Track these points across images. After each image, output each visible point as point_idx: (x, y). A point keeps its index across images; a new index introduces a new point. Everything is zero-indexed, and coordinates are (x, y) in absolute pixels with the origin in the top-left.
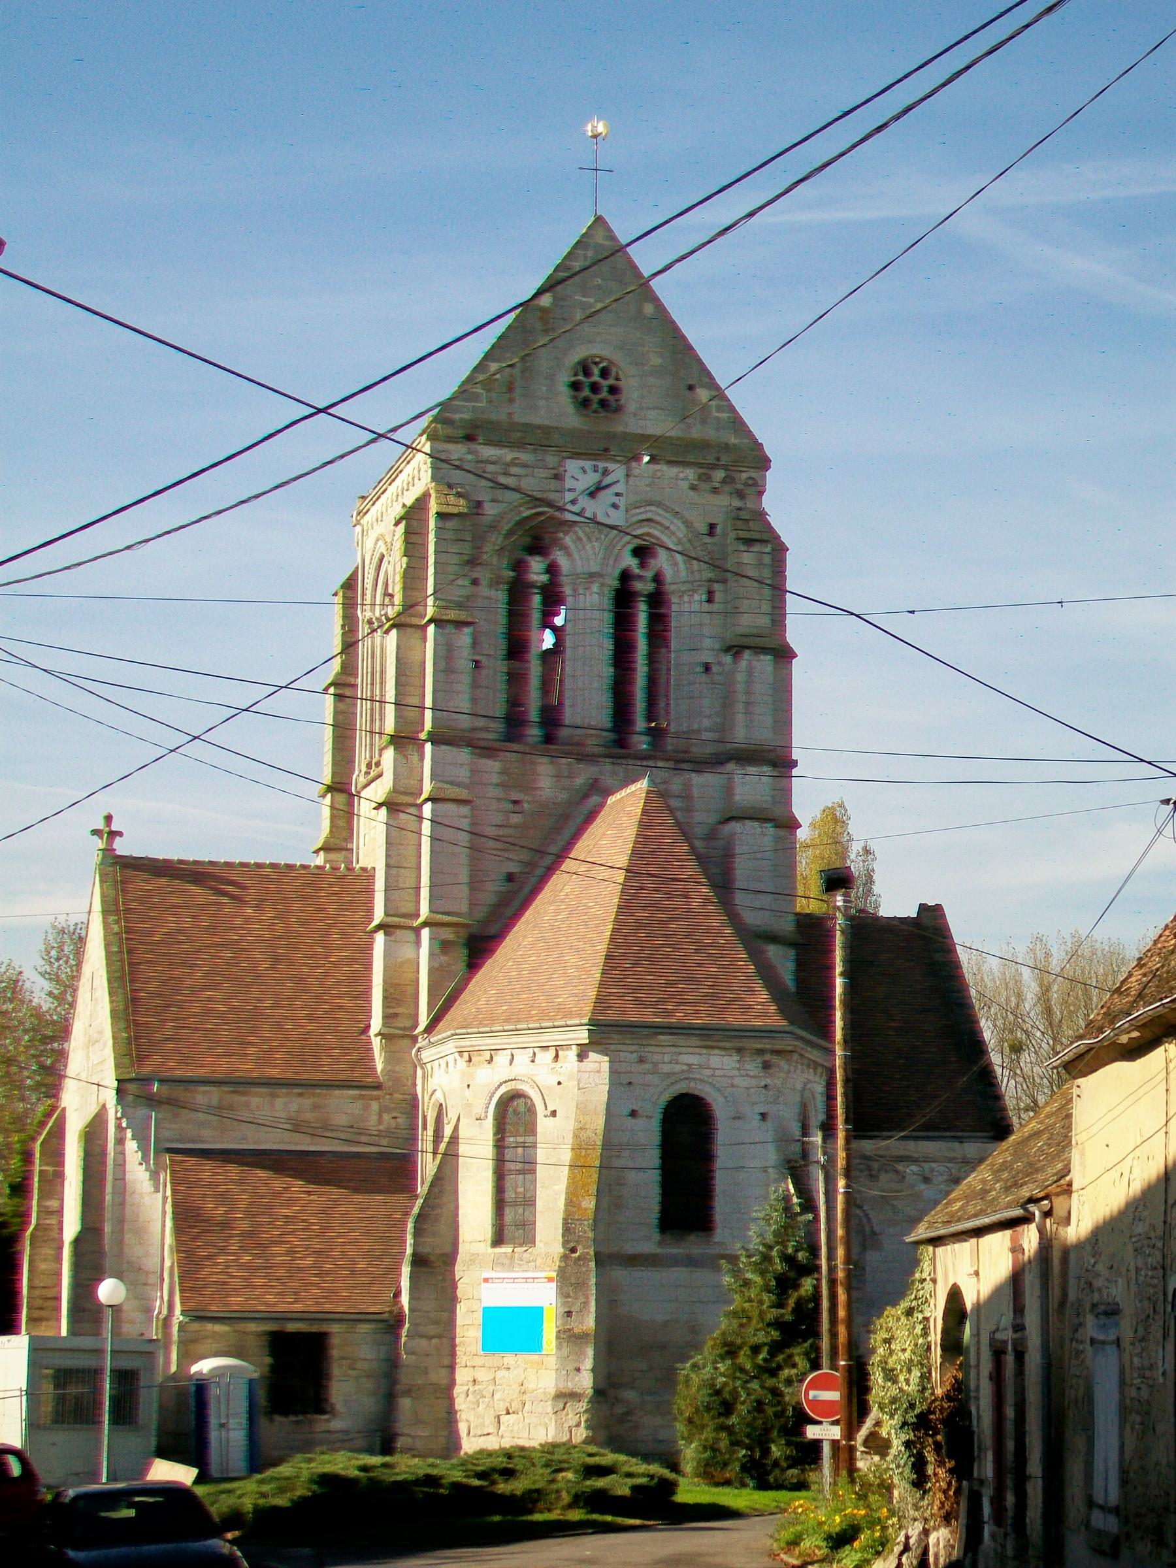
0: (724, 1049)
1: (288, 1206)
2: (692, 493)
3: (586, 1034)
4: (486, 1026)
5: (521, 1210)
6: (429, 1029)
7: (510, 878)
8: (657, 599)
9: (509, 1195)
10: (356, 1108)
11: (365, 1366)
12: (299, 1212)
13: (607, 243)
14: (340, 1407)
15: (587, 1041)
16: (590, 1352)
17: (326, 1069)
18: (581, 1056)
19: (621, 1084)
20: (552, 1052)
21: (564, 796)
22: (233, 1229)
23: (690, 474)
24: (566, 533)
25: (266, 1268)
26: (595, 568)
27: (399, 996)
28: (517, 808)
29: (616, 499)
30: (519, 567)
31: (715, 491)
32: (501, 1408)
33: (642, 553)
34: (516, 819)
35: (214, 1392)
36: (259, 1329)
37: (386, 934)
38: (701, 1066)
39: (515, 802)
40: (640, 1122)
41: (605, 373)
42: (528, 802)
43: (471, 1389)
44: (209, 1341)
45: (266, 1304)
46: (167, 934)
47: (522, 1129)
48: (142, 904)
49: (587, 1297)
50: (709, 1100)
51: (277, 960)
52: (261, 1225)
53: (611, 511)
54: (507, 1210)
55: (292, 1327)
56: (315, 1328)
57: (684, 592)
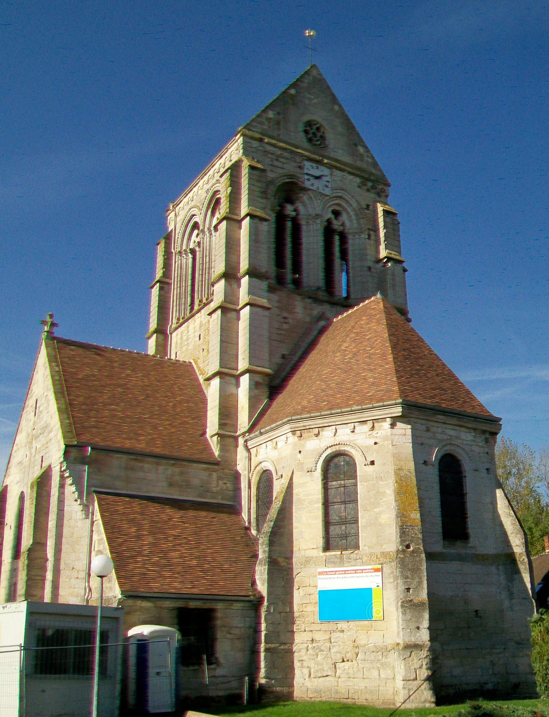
1: (174, 529)
2: (359, 189)
3: (400, 409)
5: (343, 527)
6: (251, 429)
7: (283, 356)
8: (343, 238)
9: (334, 518)
10: (204, 475)
11: (236, 631)
12: (181, 533)
13: (318, 76)
14: (222, 660)
15: (400, 414)
16: (426, 616)
17: (185, 452)
18: (393, 425)
19: (417, 443)
20: (370, 424)
21: (308, 319)
22: (143, 540)
23: (358, 180)
24: (304, 194)
25: (169, 565)
26: (319, 212)
27: (228, 413)
28: (286, 321)
29: (327, 183)
30: (282, 206)
31: (368, 190)
32: (339, 657)
33: (336, 214)
34: (286, 326)
35: (151, 648)
36: (171, 606)
38: (456, 437)
39: (285, 318)
40: (429, 468)
41: (318, 129)
43: (310, 646)
44: (139, 613)
45: (175, 588)
46: (85, 375)
47: (342, 476)
48: (70, 360)
49: (421, 578)
50: (460, 458)
51: (148, 396)
52: (160, 539)
53: (325, 188)
54: (332, 528)
55: (193, 605)
56: (208, 605)
57: (356, 233)
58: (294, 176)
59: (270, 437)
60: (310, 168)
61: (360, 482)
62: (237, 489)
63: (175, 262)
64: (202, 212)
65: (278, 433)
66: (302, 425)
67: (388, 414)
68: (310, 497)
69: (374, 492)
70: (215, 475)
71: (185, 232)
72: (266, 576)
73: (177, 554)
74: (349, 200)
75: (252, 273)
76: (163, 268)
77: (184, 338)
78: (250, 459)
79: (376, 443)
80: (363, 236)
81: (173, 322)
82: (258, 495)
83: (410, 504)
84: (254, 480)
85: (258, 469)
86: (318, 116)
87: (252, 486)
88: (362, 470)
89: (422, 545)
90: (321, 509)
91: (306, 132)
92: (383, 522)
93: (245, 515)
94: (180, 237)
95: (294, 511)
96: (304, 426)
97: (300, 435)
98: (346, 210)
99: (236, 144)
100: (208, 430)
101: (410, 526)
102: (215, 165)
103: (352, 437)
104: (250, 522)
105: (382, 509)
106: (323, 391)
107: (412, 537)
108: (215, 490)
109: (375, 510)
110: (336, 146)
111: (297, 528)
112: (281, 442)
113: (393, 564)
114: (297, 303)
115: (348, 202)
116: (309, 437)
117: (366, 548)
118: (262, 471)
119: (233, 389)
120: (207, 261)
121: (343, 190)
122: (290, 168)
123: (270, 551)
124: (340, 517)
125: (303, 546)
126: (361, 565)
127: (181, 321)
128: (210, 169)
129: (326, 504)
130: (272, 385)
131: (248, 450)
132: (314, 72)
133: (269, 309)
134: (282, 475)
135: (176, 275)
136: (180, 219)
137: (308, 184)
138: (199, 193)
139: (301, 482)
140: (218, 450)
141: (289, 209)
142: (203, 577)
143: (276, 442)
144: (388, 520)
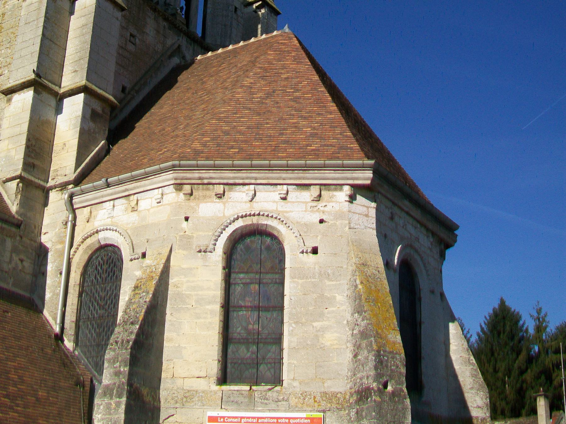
0: (428, 229)
4: (228, 157)
9: (237, 330)
15: (368, 182)
18: (352, 198)
20: (315, 191)
34: (131, 47)
37: (35, 91)
39: (132, 35)
42: (139, 40)
50: (417, 270)
59: (126, 190)
61: (292, 278)
62: (40, 273)
65: (145, 186)
66: (197, 175)
67: (348, 179)
68: (200, 293)
69: (315, 296)
72: (123, 416)
79: (321, 221)
82: (82, 285)
83: (385, 319)
84: (79, 259)
85: (89, 241)
88: (292, 259)
89: (405, 385)
90: (218, 314)
92: (328, 344)
93: (51, 314)
95: (168, 311)
96: (200, 178)
97: (190, 192)
101: (390, 352)
103: (282, 206)
104: (62, 328)
105: (326, 323)
106: (227, 133)
107: (392, 370)
109: (315, 324)
111: (171, 340)
112: (147, 202)
113: (342, 412)
116: (205, 197)
117: (296, 384)
118: (97, 246)
119: (49, 113)
123: (131, 374)
124: (249, 332)
125: (180, 371)
126: (285, 411)
129: (227, 308)
130: (118, 119)
133: (122, 9)
134: (144, 255)
139: (184, 266)
140: (16, 203)
142: (11, 408)
143: (138, 201)
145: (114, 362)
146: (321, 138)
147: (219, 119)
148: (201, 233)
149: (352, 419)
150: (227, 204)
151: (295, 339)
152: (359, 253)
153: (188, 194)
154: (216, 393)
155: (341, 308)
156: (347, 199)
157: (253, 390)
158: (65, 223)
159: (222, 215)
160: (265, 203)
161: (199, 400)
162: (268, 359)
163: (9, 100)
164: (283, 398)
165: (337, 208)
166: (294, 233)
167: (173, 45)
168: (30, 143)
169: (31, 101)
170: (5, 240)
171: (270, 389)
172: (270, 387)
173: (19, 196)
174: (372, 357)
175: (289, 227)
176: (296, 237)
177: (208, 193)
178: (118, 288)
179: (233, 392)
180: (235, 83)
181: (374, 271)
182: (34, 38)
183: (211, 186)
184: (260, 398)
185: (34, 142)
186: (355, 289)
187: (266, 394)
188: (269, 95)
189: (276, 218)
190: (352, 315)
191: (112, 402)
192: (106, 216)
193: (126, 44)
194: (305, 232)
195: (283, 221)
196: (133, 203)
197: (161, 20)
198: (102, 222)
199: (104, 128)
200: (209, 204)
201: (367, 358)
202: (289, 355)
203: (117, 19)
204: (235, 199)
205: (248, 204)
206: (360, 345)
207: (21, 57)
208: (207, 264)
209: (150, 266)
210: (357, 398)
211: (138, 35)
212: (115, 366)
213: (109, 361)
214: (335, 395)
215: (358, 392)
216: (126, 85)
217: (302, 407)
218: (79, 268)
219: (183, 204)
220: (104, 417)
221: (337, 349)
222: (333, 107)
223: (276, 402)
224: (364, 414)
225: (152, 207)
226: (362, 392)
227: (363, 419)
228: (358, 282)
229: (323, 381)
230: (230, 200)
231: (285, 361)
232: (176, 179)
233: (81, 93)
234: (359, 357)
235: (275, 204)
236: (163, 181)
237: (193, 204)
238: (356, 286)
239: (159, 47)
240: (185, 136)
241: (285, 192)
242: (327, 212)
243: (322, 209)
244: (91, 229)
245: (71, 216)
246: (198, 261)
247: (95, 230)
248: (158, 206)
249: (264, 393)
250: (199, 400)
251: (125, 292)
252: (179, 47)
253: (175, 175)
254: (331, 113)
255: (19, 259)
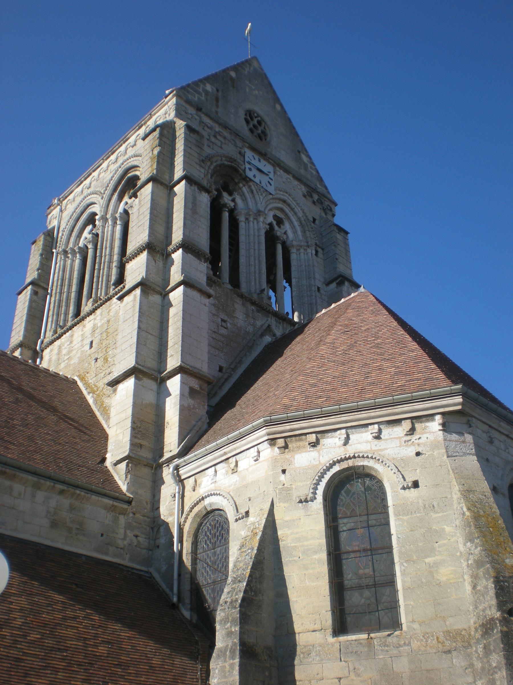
2: (304, 199)
6: (184, 452)
9: (349, 578)
15: (459, 407)
20: (407, 425)
23: (304, 188)
28: (224, 324)
34: (223, 331)
37: (136, 378)
39: (223, 320)
41: (259, 123)
42: (230, 323)
58: (235, 161)
59: (225, 454)
60: (252, 158)
61: (396, 515)
63: (56, 264)
64: (104, 196)
68: (305, 543)
70: (122, 520)
71: (74, 227)
72: (237, 677)
73: (70, 632)
74: (294, 207)
75: (186, 246)
76: (38, 270)
77: (64, 352)
78: (183, 497)
79: (418, 454)
80: (309, 251)
81: (47, 332)
85: (196, 509)
86: (261, 109)
87: (185, 538)
91: (247, 122)
92: (444, 579)
94: (66, 233)
97: (283, 445)
98: (289, 218)
99: (166, 107)
100: (108, 456)
102: (129, 138)
108: (120, 543)
109: (427, 560)
110: (278, 145)
112: (246, 462)
114: (237, 306)
115: (292, 209)
116: (299, 448)
118: (204, 513)
120: (107, 253)
121: (287, 193)
122: (230, 150)
127: (59, 331)
128: (121, 145)
131: (180, 481)
132: (255, 64)
134: (247, 513)
135: (56, 279)
136: (66, 215)
137: (250, 174)
138: (101, 176)
139: (287, 518)
141: (226, 198)
143: (237, 462)
144: (452, 576)
145: (225, 623)
146: (406, 374)
147: (307, 375)
148: (299, 484)
149: (481, 656)
150: (321, 452)
151: (408, 579)
152: (462, 480)
153: (283, 447)
154: (333, 645)
155: (452, 540)
156: (441, 428)
157: (371, 638)
158: (173, 496)
159: (318, 463)
160: (359, 445)
161: (316, 655)
162: (383, 603)
163: (115, 391)
164: (404, 643)
165: (432, 439)
166: (392, 470)
167: (262, 326)
168: (136, 425)
169: (133, 388)
170: (118, 518)
171: (389, 635)
172: (389, 633)
173: (129, 476)
174: (491, 585)
175: (386, 464)
176: (395, 473)
177: (301, 443)
178: (227, 550)
179: (353, 642)
180: (320, 342)
181: (480, 496)
182: (132, 332)
183: (304, 437)
184: (380, 645)
185: (139, 425)
186: (463, 518)
187: (386, 641)
188: (351, 347)
189: (372, 458)
190: (465, 544)
191: (227, 665)
192: (210, 482)
193: (218, 329)
194: (403, 467)
195: (379, 460)
196: (233, 465)
197: (248, 305)
198: (207, 489)
199: (203, 403)
200: (304, 454)
201: (486, 587)
202: (404, 597)
203: (205, 305)
204: (329, 445)
205: (343, 448)
206: (477, 575)
207: (122, 351)
208: (309, 513)
209: (253, 523)
210: (482, 631)
211: (229, 320)
212: (226, 627)
213: (220, 624)
214: (458, 633)
215: (483, 625)
216: (222, 365)
217: (425, 650)
218: (190, 537)
219: (279, 457)
220: (220, 681)
221: (454, 583)
222: (414, 345)
223: (397, 647)
224: (492, 648)
225: (250, 466)
226: (486, 625)
227: (491, 653)
228: (465, 509)
229: (444, 619)
230: (324, 447)
231: (401, 602)
232: (269, 434)
233: (177, 374)
234: (479, 588)
235: (369, 444)
236: (257, 439)
237: (287, 455)
238: (464, 514)
239: (250, 329)
240: (276, 395)
241: (376, 431)
242: (422, 444)
243: (417, 441)
244: (197, 497)
245: (177, 487)
246: (299, 511)
247: (201, 498)
248: (255, 464)
249: (383, 640)
250: (316, 655)
251: (234, 553)
252: (269, 326)
253: (267, 430)
254: (413, 351)
255: (134, 536)
